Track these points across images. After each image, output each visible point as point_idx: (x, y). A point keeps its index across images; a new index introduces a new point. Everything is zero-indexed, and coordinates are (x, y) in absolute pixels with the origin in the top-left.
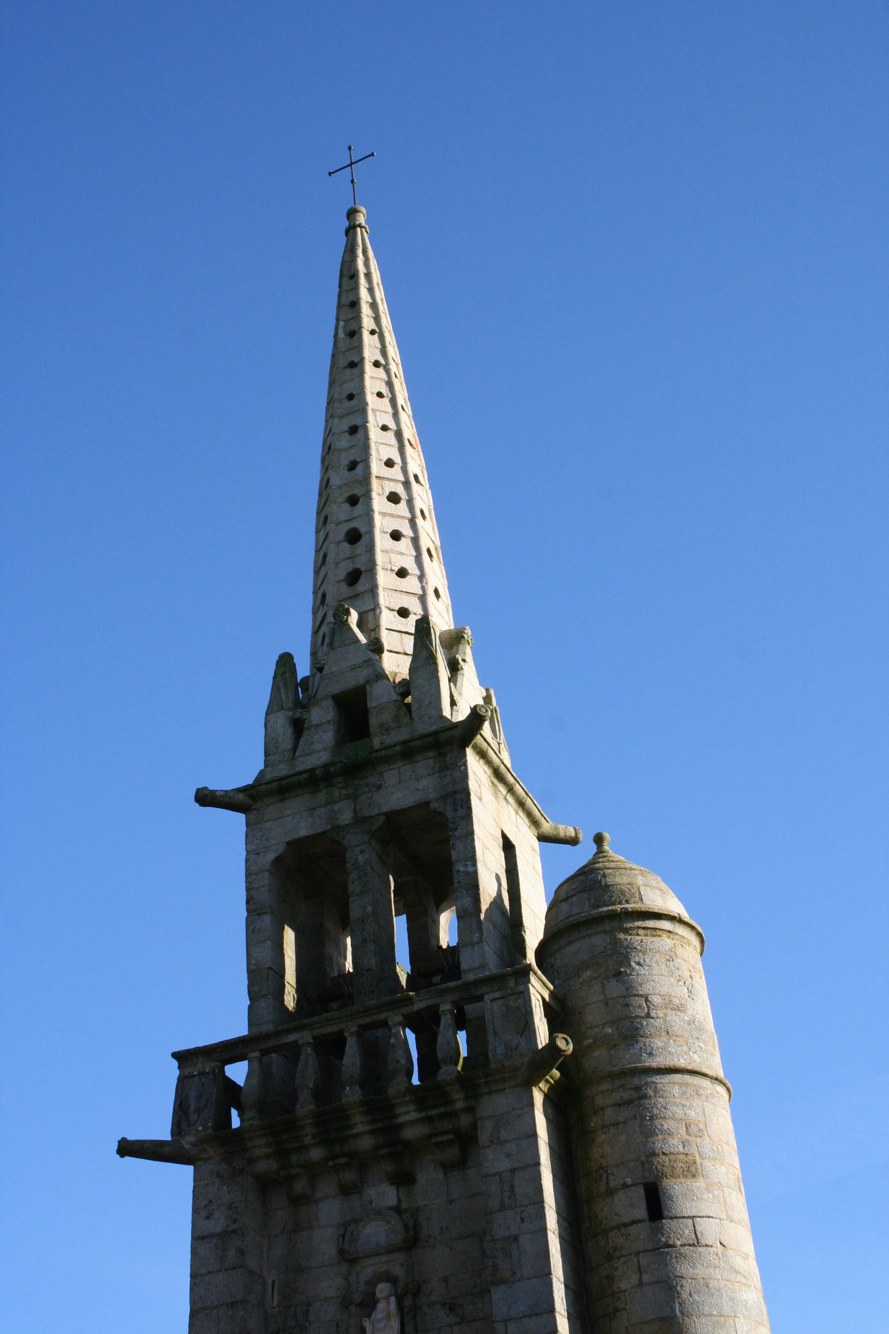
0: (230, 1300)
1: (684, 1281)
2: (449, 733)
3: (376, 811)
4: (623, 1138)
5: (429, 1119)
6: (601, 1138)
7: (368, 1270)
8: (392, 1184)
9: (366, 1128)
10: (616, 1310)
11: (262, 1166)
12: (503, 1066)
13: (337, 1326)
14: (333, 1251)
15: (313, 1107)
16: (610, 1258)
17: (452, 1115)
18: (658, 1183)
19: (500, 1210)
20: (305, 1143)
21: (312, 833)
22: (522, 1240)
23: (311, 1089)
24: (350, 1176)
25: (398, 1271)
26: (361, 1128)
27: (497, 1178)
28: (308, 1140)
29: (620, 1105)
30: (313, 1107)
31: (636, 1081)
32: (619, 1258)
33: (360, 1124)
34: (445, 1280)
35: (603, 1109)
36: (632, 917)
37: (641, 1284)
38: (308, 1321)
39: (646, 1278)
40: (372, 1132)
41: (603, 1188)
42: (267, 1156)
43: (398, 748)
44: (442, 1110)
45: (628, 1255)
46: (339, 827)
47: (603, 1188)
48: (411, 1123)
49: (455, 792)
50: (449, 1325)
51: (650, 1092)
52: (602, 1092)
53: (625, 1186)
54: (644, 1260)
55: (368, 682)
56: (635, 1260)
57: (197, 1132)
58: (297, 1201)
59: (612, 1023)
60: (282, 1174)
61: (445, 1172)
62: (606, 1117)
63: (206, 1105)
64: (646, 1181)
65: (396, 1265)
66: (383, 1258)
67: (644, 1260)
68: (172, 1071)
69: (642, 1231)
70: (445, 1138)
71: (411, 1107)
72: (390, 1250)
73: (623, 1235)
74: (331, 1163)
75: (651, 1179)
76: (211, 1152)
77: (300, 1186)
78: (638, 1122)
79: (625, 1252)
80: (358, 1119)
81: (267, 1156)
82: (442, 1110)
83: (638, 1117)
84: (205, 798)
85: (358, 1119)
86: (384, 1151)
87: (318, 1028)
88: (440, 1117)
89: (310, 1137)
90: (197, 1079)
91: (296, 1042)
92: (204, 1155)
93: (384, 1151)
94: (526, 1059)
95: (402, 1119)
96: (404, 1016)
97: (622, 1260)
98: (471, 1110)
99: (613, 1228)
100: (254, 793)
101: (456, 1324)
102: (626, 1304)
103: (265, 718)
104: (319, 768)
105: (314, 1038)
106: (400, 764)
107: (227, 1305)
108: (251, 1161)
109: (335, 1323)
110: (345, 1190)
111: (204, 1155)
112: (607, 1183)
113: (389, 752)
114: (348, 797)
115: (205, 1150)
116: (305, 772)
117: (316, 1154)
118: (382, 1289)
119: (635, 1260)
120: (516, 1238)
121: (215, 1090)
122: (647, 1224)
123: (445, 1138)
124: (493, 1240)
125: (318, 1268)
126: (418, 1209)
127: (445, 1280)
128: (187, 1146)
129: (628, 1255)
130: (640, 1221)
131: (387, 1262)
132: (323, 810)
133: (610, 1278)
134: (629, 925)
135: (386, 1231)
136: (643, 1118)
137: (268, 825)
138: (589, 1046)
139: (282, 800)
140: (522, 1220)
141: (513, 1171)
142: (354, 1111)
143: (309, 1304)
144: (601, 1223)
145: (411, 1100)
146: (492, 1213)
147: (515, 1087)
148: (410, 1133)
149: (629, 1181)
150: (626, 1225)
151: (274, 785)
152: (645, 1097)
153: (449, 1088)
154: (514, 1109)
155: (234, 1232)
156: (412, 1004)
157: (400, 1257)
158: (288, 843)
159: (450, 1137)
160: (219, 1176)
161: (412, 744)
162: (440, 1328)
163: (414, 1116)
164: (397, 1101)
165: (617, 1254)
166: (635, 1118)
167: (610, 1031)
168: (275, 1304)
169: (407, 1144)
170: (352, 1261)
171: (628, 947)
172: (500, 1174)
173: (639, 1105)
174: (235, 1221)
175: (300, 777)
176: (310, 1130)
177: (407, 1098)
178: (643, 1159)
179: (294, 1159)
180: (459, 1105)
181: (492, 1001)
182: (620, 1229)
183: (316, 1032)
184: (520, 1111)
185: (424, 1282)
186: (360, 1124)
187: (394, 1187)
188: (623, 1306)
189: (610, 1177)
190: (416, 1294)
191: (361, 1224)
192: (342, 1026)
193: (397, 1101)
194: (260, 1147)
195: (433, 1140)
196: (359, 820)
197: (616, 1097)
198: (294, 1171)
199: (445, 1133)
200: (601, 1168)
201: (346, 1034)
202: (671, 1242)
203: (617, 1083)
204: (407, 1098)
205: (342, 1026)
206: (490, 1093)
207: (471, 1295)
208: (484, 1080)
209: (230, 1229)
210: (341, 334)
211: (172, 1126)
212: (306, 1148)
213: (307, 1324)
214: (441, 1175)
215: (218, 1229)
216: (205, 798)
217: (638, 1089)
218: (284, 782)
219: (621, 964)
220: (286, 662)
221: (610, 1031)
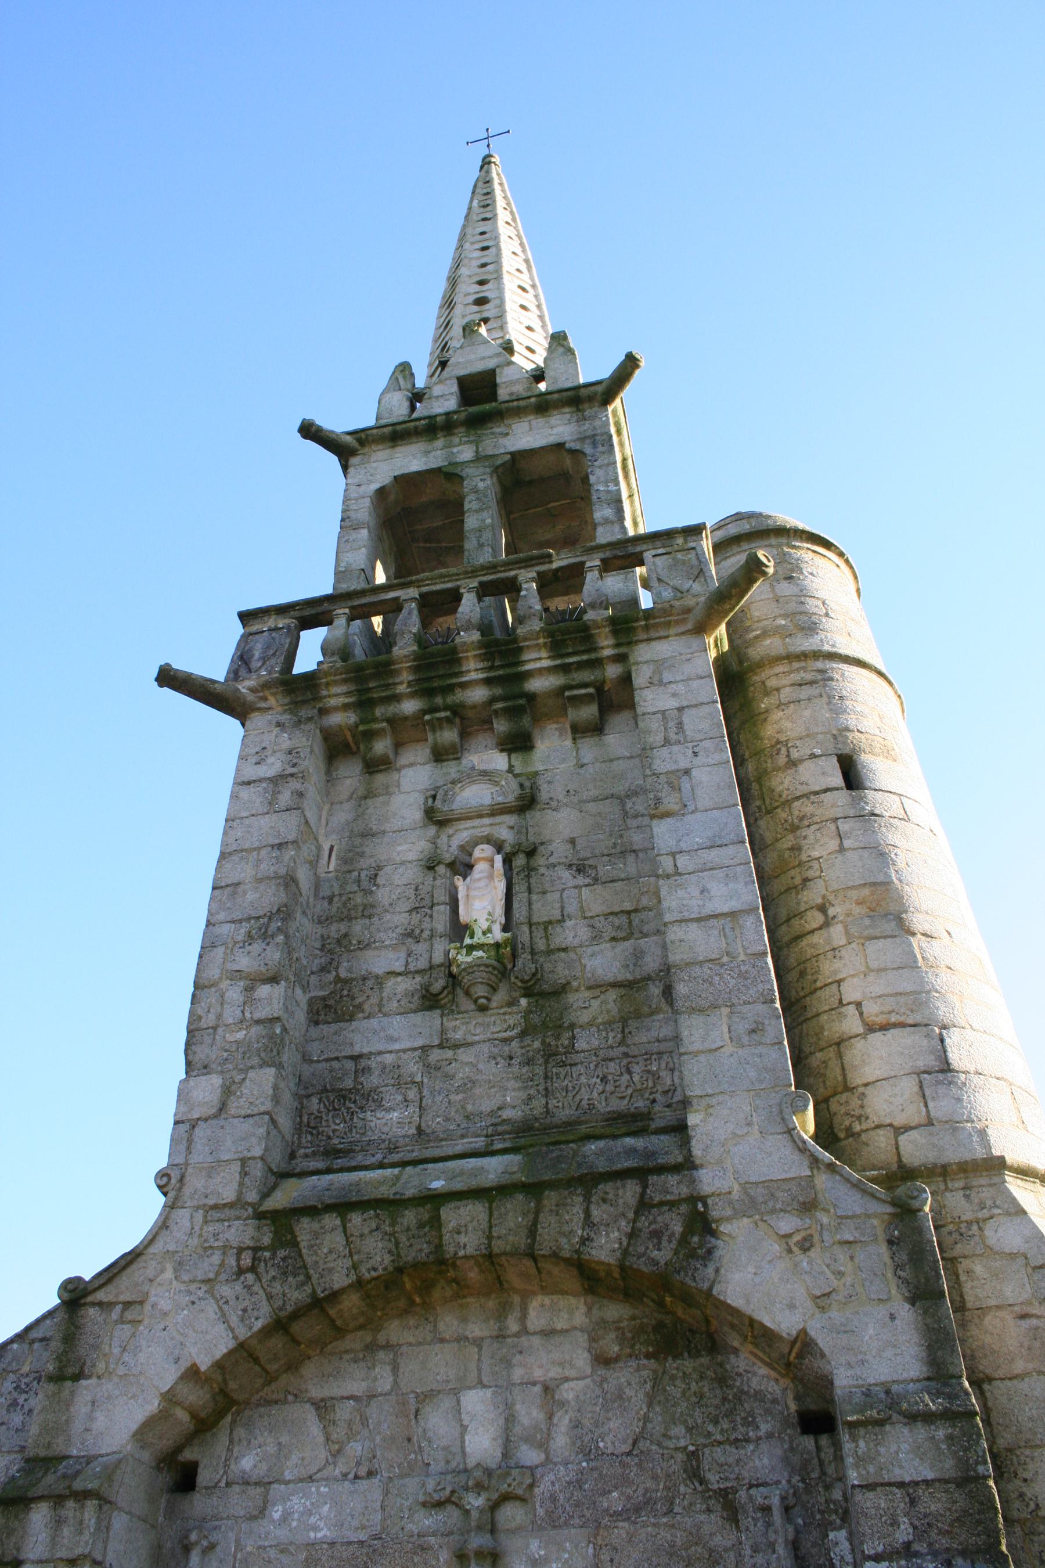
0: (277, 841)
1: (897, 850)
2: (592, 389)
3: (502, 451)
4: (807, 713)
5: (565, 669)
6: (776, 715)
7: (461, 834)
8: (502, 751)
9: (482, 676)
10: (806, 880)
11: (337, 719)
12: (671, 606)
13: (416, 889)
14: (418, 815)
15: (415, 648)
16: (794, 829)
17: (597, 663)
18: (855, 757)
19: (663, 746)
20: (398, 691)
21: (424, 468)
22: (694, 773)
23: (414, 634)
24: (449, 736)
25: (505, 834)
26: (473, 676)
27: (660, 716)
28: (402, 689)
29: (800, 685)
30: (415, 648)
31: (819, 665)
32: (809, 826)
33: (473, 669)
34: (572, 841)
35: (778, 690)
36: (801, 538)
37: (842, 849)
38: (375, 885)
39: (847, 843)
40: (488, 682)
41: (782, 760)
42: (346, 707)
43: (533, 400)
44: (585, 657)
45: (822, 822)
46: (456, 463)
47: (782, 760)
48: (540, 671)
49: (594, 435)
50: (576, 887)
51: (836, 676)
52: (777, 675)
53: (813, 756)
54: (844, 826)
55: (498, 366)
56: (833, 827)
57: (259, 676)
58: (375, 766)
59: (785, 616)
60: (361, 728)
61: (574, 739)
62: (782, 696)
63: (274, 654)
64: (840, 752)
65: (504, 829)
66: (487, 821)
67: (844, 826)
68: (238, 630)
69: (843, 797)
70: (583, 691)
71: (544, 654)
72: (496, 811)
73: (813, 803)
74: (427, 717)
75: (846, 751)
76: (272, 701)
77: (381, 746)
78: (825, 699)
79: (817, 819)
80: (472, 664)
81: (346, 707)
82: (585, 657)
83: (824, 695)
84: (309, 431)
85: (472, 664)
86: (499, 705)
87: (428, 585)
88: (580, 666)
89: (405, 685)
90: (265, 634)
91: (397, 599)
92: (263, 705)
93: (499, 705)
94: (702, 599)
95: (528, 667)
96: (538, 573)
97: (813, 828)
98: (621, 658)
99: (798, 798)
100: (363, 436)
101: (586, 886)
102: (822, 872)
103: (194, 996)
104: (440, 415)
105: (420, 595)
106: (531, 417)
107: (273, 846)
108: (323, 712)
109: (413, 887)
110: (440, 755)
111: (263, 705)
112: (788, 756)
113: (522, 403)
114: (471, 442)
115: (265, 699)
116: (424, 418)
117: (410, 707)
118: (482, 851)
119: (833, 827)
120: (687, 772)
121: (288, 641)
122: (845, 792)
123: (583, 691)
124: (654, 774)
125: (394, 832)
126: (536, 774)
127: (572, 841)
128: (244, 691)
129: (822, 822)
130: (837, 789)
131: (491, 825)
132: (439, 452)
133: (796, 849)
134: (797, 544)
135: (492, 793)
136: (830, 697)
137: (374, 465)
138: (756, 637)
139: (393, 447)
140: (695, 754)
141: (680, 709)
142: (469, 654)
143: (379, 868)
144: (780, 796)
145: (545, 644)
146: (652, 749)
147: (683, 633)
148: (536, 685)
149: (818, 752)
150: (816, 793)
151: (386, 430)
152: (831, 679)
153: (597, 631)
154: (681, 654)
155: (292, 775)
156: (551, 562)
157: (510, 819)
158: (395, 477)
159: (591, 690)
160: (278, 724)
161: (548, 397)
162: (564, 890)
163: (546, 663)
164: (527, 643)
165: (806, 823)
166: (821, 696)
167: (783, 622)
168: (331, 868)
169: (531, 697)
170: (442, 824)
171: (798, 559)
172: (663, 713)
173: (825, 686)
174: (294, 765)
175: (418, 423)
176: (406, 676)
177: (541, 641)
178: (835, 732)
179: (379, 711)
180: (607, 652)
181: (654, 556)
182: (808, 798)
183: (425, 589)
184: (689, 656)
185: (542, 844)
186: (473, 669)
187: (505, 755)
188: (818, 873)
189: (791, 750)
190: (531, 853)
191: (460, 785)
192: (458, 583)
193: (527, 643)
194: (337, 695)
195: (567, 694)
196: (478, 459)
197: (795, 677)
198: (376, 726)
199: (585, 685)
200: (778, 742)
201: (462, 591)
202: (877, 812)
203: (796, 665)
204: (541, 641)
205: (458, 583)
206: (649, 640)
207: (608, 855)
208: (643, 623)
209: (286, 772)
210: (475, 203)
211: (228, 673)
212: (396, 698)
213: (374, 888)
214: (568, 743)
215: (271, 772)
216: (309, 431)
217: (822, 671)
218: (399, 428)
219: (792, 570)
220: (404, 369)
221: (783, 622)
